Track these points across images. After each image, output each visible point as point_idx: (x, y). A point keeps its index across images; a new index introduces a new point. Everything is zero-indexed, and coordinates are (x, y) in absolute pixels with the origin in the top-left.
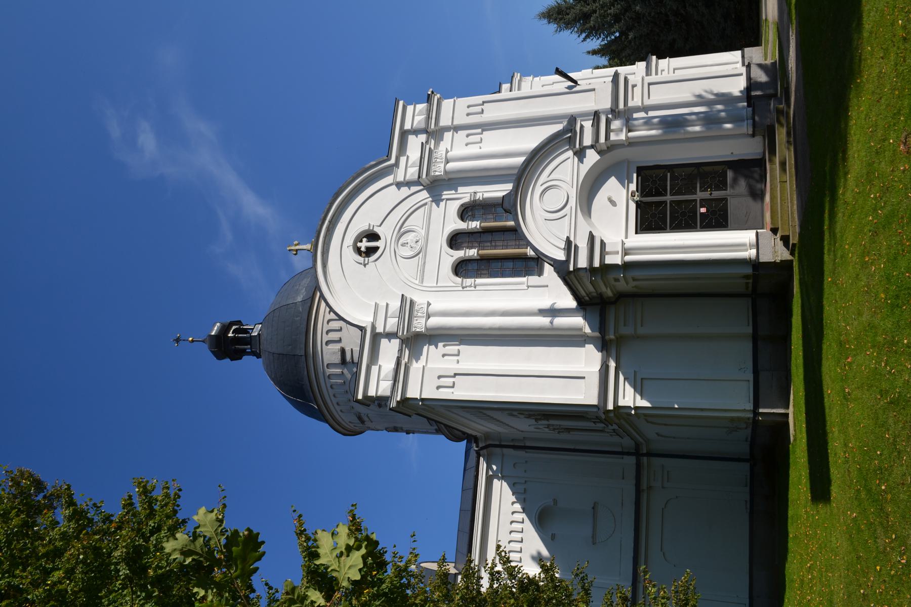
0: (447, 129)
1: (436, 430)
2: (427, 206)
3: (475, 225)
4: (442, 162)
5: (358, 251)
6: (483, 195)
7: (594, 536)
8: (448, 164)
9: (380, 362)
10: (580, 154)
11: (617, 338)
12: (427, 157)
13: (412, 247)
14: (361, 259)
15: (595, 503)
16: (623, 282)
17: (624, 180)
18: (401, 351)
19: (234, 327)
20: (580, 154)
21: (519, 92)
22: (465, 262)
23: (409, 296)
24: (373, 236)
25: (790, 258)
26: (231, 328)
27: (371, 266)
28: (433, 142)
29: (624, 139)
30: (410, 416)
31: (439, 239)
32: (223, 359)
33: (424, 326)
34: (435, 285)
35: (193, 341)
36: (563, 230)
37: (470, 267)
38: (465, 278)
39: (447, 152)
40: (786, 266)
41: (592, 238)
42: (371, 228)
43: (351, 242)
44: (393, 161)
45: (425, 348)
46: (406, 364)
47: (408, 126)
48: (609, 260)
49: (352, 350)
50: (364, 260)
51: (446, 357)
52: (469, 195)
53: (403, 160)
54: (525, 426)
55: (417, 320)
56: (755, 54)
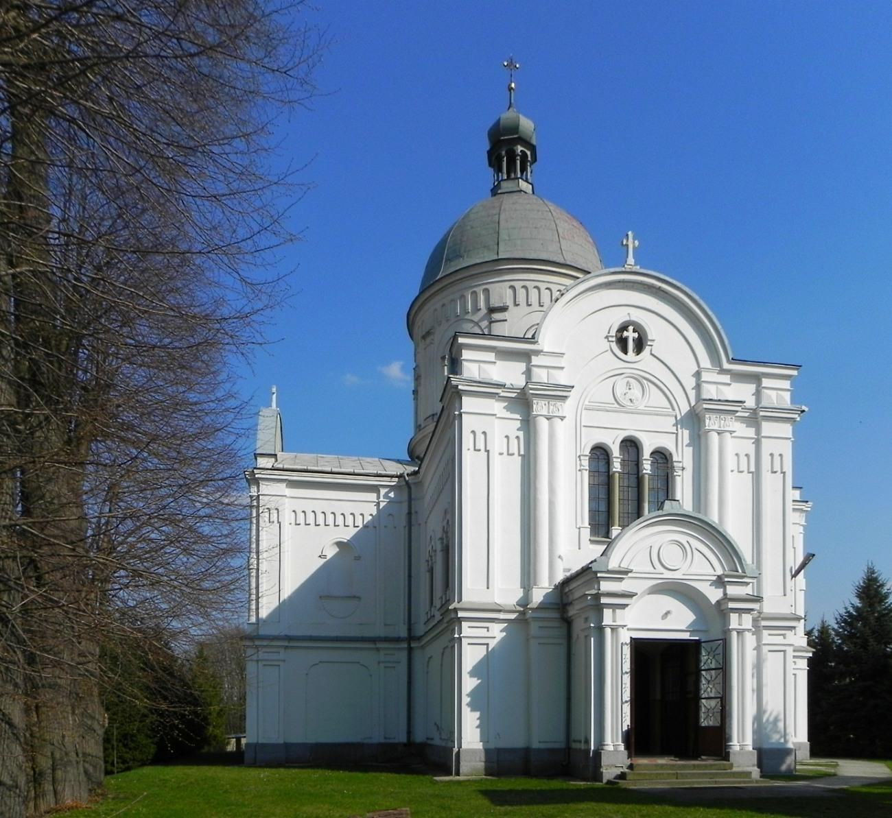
0: (758, 432)
1: (420, 426)
2: (671, 410)
3: (647, 467)
4: (720, 427)
5: (623, 328)
6: (679, 476)
7: (329, 597)
8: (716, 434)
9: (499, 363)
10: (720, 582)
11: (526, 620)
12: (728, 408)
13: (625, 394)
14: (613, 333)
15: (359, 598)
16: (584, 626)
17: (692, 629)
18: (512, 388)
19: (529, 153)
20: (720, 582)
21: (791, 510)
22: (606, 457)
23: (573, 394)
24: (640, 345)
25: (605, 781)
26: (528, 149)
27: (606, 344)
28: (747, 415)
29: (730, 627)
30: (441, 400)
31: (631, 426)
32: (490, 139)
33: (539, 413)
34: (583, 424)
35: (510, 89)
36: (639, 565)
37: (602, 463)
38: (589, 458)
39: (731, 432)
40: (597, 776)
41: (630, 595)
42: (649, 343)
43: (633, 318)
44: (726, 366)
45: (518, 417)
46: (497, 394)
47: (766, 382)
48: (607, 613)
49: (506, 320)
50: (612, 337)
51: (506, 440)
52: (680, 460)
53: (726, 378)
54: (432, 526)
55: (545, 404)
56: (804, 754)
